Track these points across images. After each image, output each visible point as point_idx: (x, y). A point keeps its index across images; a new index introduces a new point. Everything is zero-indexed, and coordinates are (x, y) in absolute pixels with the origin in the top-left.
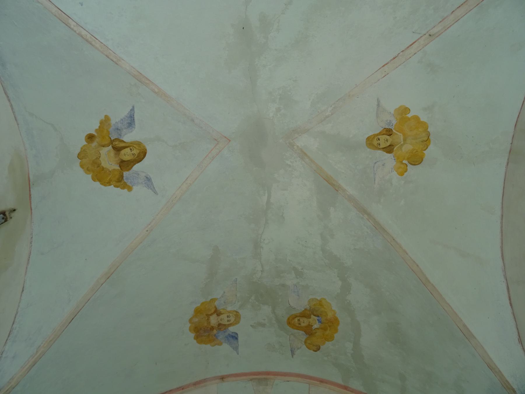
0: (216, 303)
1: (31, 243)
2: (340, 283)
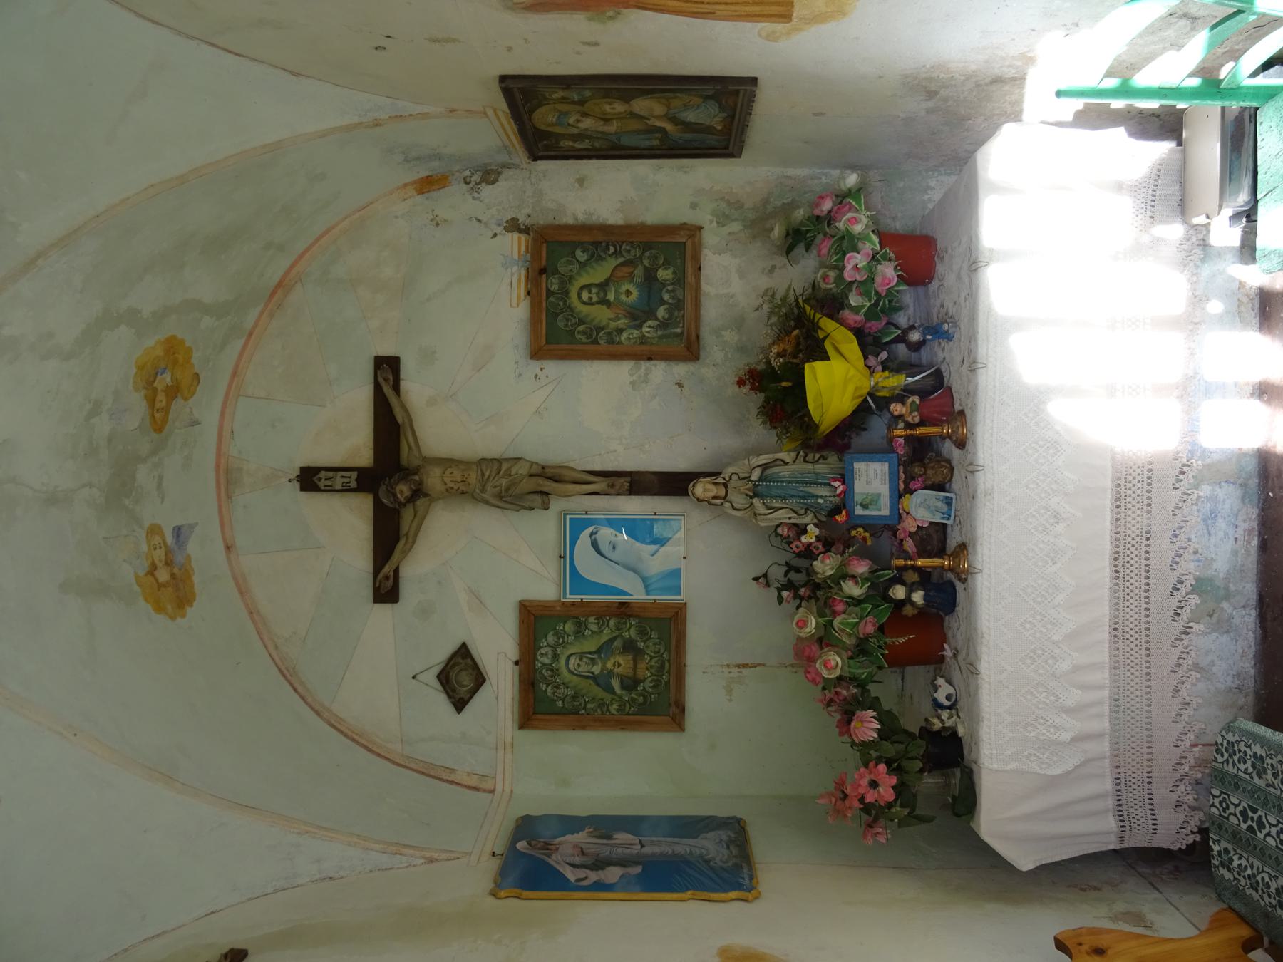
0: (141, 573)
1: (126, 950)
2: (123, 328)
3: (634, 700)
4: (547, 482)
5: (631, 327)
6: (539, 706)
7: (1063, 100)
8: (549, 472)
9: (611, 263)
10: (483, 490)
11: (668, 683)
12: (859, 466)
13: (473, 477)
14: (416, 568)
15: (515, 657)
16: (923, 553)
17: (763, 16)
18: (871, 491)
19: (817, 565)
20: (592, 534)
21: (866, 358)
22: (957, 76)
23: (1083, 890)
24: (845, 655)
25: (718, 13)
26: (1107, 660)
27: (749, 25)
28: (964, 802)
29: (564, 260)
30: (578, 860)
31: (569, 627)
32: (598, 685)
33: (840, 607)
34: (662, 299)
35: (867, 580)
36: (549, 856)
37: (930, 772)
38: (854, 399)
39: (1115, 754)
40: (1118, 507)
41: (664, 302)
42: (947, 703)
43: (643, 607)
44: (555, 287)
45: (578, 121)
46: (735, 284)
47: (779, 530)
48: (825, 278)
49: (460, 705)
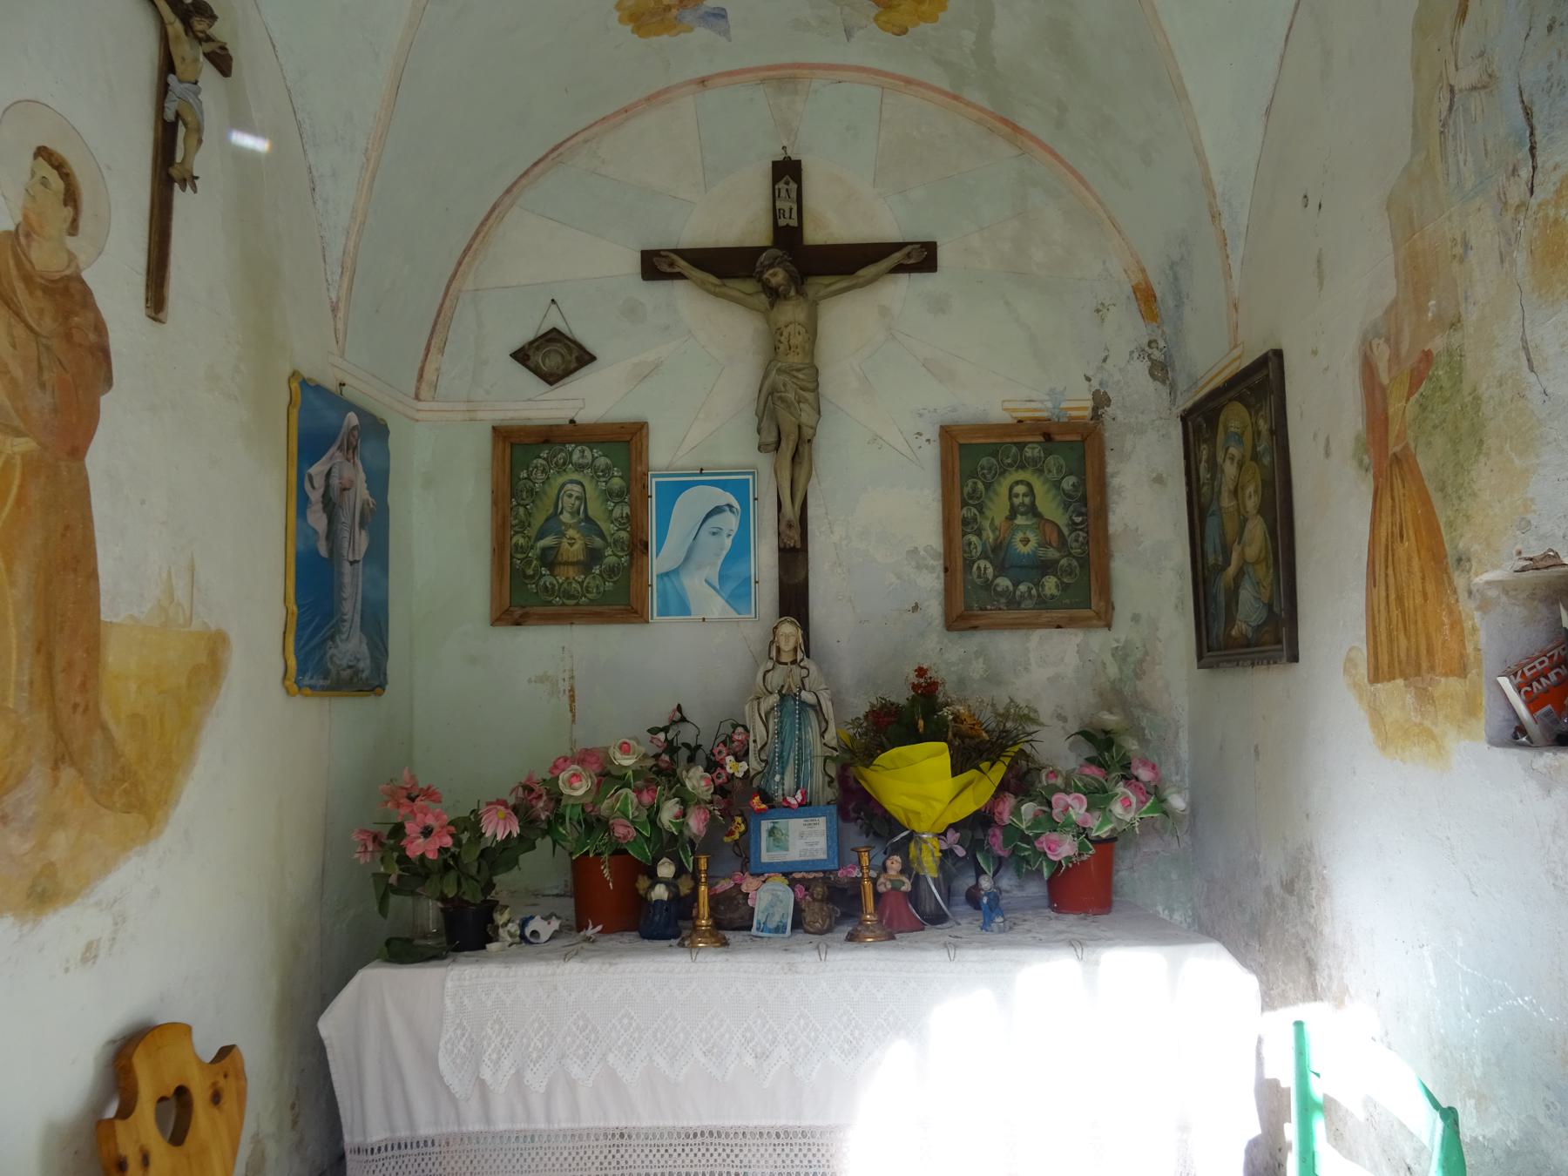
3: (529, 563)
4: (791, 446)
5: (984, 545)
6: (521, 451)
7: (1291, 1030)
8: (804, 449)
9: (1061, 519)
10: (779, 371)
11: (550, 603)
12: (821, 823)
13: (795, 359)
14: (685, 301)
15: (578, 420)
16: (715, 900)
17: (1375, 648)
18: (790, 839)
19: (698, 771)
20: (730, 506)
21: (954, 826)
22: (1314, 912)
23: (293, 1107)
24: (589, 799)
25: (1375, 591)
26: (584, 1125)
27: (1364, 633)
28: (405, 950)
29: (1062, 462)
30: (335, 481)
31: (617, 483)
32: (547, 520)
33: (646, 798)
34: (1020, 583)
35: (681, 832)
36: (340, 448)
37: (442, 910)
38: (906, 811)
39: (463, 1138)
40: (778, 1135)
41: (1016, 584)
42: (528, 932)
43: (643, 571)
44: (1028, 452)
45: (1232, 459)
46: (1041, 671)
47: (740, 729)
48: (1054, 773)
49: (521, 356)
